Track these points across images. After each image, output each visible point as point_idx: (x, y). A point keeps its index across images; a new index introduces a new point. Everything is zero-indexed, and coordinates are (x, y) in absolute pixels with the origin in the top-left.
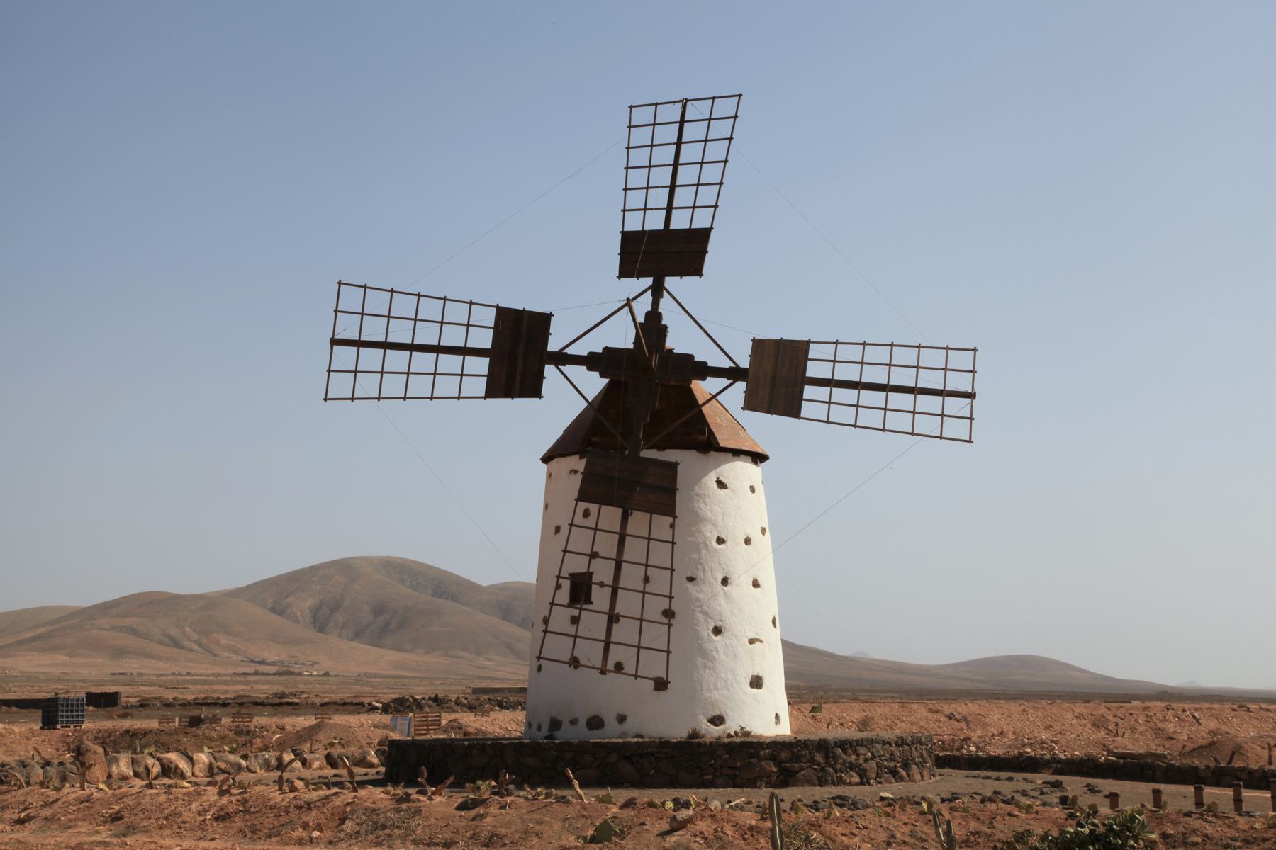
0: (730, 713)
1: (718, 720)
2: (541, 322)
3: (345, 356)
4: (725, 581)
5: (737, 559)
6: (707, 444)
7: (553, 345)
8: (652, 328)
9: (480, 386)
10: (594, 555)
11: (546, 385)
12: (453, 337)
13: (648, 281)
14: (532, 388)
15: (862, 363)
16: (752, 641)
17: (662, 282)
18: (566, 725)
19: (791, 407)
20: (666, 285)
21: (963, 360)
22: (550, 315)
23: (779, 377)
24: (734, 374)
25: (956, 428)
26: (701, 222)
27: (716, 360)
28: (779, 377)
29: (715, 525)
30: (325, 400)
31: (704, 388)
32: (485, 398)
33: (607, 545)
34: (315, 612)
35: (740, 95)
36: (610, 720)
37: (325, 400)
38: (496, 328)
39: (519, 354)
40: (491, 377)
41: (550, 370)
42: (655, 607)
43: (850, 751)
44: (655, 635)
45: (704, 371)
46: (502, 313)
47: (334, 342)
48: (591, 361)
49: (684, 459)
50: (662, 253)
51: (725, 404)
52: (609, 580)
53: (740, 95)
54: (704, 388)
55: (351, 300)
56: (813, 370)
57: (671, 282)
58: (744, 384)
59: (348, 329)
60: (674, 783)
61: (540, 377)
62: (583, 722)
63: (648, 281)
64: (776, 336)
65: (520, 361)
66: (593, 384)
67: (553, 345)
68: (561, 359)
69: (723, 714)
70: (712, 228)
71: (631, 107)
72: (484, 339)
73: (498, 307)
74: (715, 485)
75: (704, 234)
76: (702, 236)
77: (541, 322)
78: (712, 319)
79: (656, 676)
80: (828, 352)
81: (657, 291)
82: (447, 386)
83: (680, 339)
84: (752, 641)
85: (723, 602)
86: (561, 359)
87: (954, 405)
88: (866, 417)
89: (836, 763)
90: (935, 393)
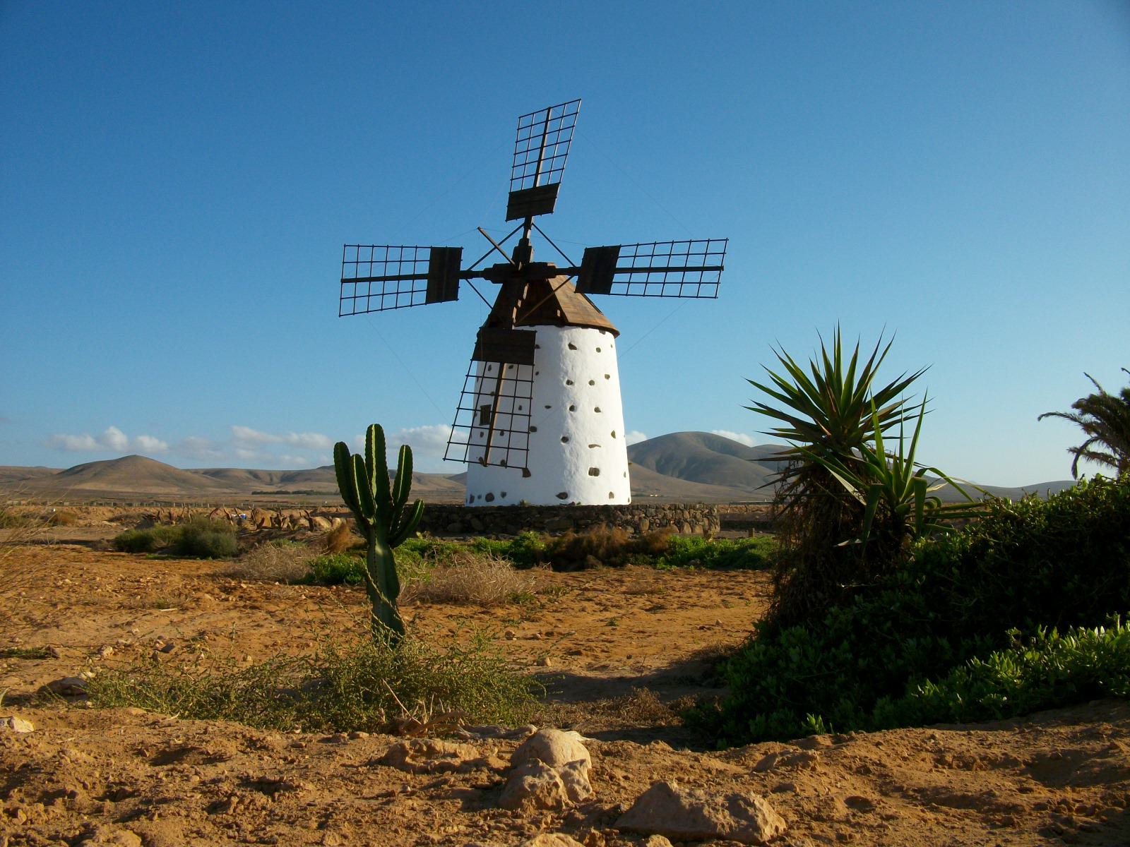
0: (572, 491)
1: (563, 496)
2: (456, 254)
4: (572, 408)
5: (584, 397)
6: (563, 322)
7: (464, 267)
8: (523, 249)
9: (422, 297)
12: (407, 270)
13: (522, 221)
14: (452, 295)
15: (357, 262)
16: (591, 446)
19: (604, 288)
20: (533, 221)
21: (716, 247)
22: (462, 248)
23: (598, 270)
24: (571, 272)
25: (708, 290)
27: (561, 264)
28: (598, 270)
29: (566, 373)
30: (340, 316)
31: (554, 282)
32: (426, 304)
36: (497, 495)
38: (431, 261)
39: (444, 275)
41: (462, 282)
42: (521, 423)
44: (518, 440)
45: (554, 272)
47: (343, 281)
49: (543, 333)
50: (531, 203)
51: (565, 291)
54: (554, 282)
56: (620, 264)
57: (534, 219)
58: (461, 269)
61: (457, 287)
62: (484, 497)
63: (522, 221)
64: (600, 245)
66: (492, 290)
67: (464, 267)
68: (469, 275)
69: (567, 491)
70: (472, 360)
72: (424, 268)
73: (431, 248)
74: (567, 347)
76: (551, 190)
77: (456, 254)
78: (559, 241)
80: (631, 251)
81: (527, 226)
82: (404, 300)
84: (591, 446)
85: (570, 421)
86: (469, 275)
87: (709, 276)
88: (669, 289)
89: (615, 520)
90: (698, 269)
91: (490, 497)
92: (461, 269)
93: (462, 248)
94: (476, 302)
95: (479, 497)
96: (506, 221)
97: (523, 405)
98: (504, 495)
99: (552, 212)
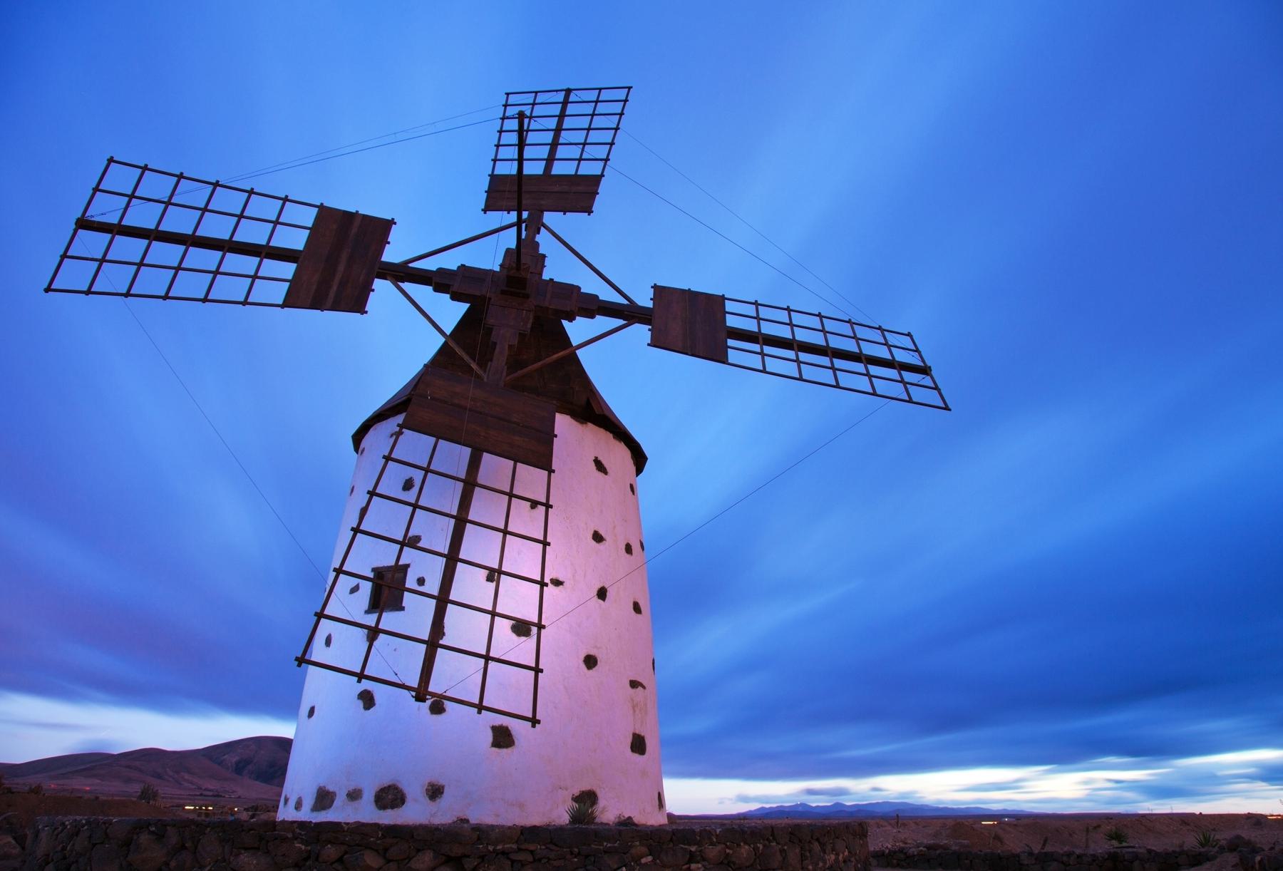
2: (380, 229)
3: (93, 243)
7: (393, 254)
8: (524, 260)
9: (279, 292)
10: (411, 542)
11: (373, 302)
17: (541, 217)
18: (340, 799)
22: (392, 222)
26: (588, 169)
32: (283, 306)
33: (437, 533)
34: (237, 763)
35: (630, 88)
36: (414, 790)
37: (48, 290)
40: (295, 283)
41: (379, 284)
43: (829, 847)
46: (326, 214)
47: (84, 224)
48: (441, 281)
52: (433, 587)
53: (630, 88)
55: (121, 179)
59: (106, 209)
60: (302, 825)
61: (367, 289)
65: (341, 268)
68: (402, 274)
70: (602, 175)
71: (508, 94)
73: (321, 208)
75: (596, 180)
77: (380, 229)
79: (603, 187)
81: (536, 225)
83: (559, 268)
86: (402, 274)
91: (390, 797)
92: (383, 259)
93: (392, 222)
94: (400, 335)
95: (354, 795)
96: (485, 211)
97: (601, 546)
98: (435, 792)
99: (590, 212)
